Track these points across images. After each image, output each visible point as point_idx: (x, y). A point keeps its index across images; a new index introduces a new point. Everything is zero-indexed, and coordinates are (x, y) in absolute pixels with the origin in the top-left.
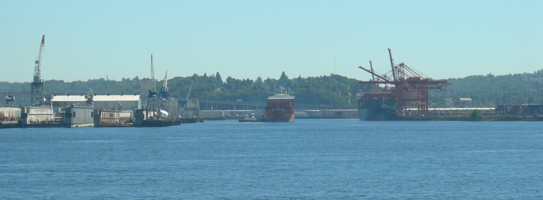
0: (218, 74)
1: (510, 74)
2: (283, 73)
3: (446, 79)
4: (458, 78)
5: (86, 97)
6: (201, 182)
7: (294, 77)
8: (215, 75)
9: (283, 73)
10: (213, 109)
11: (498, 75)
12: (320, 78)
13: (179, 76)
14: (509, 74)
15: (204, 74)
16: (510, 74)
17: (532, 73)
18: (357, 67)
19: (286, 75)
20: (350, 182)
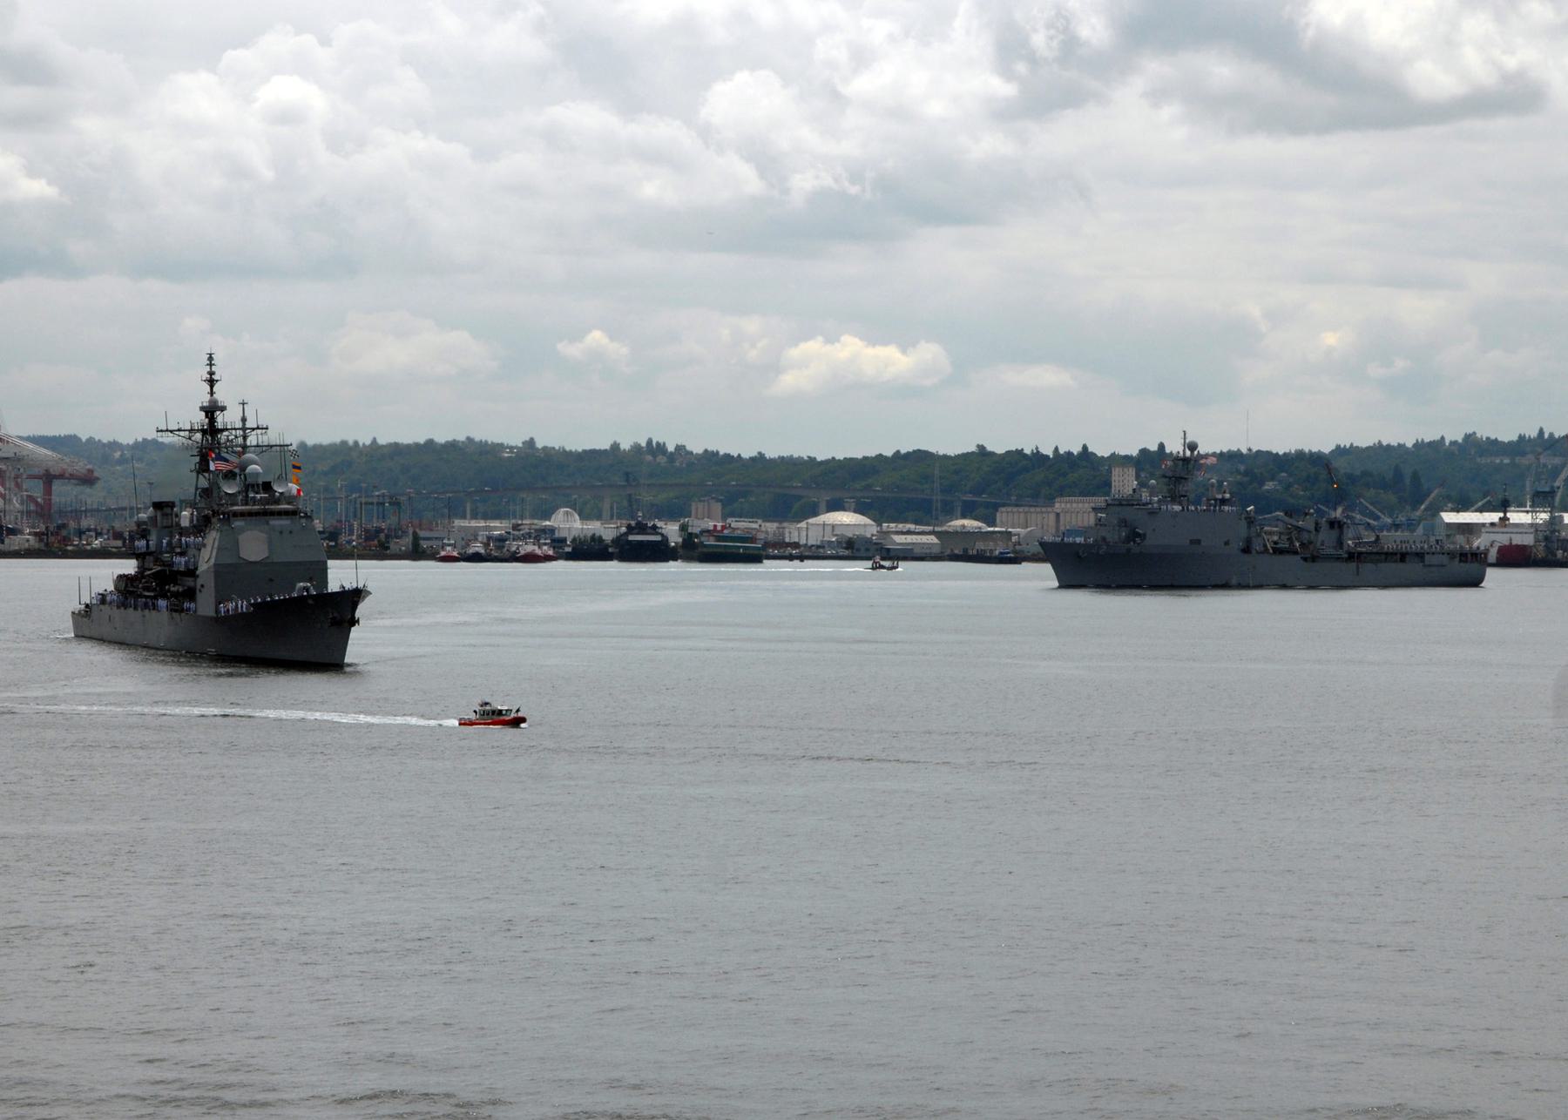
0: (532, 439)
1: (615, 446)
2: (375, 439)
3: (1232, 449)
4: (1463, 436)
5: (299, 491)
6: (24, 970)
7: (834, 456)
8: (644, 444)
9: (375, 439)
10: (165, 570)
11: (1360, 446)
12: (1413, 449)
13: (926, 449)
14: (1377, 442)
15: (1080, 449)
16: (615, 446)
17: (1345, 446)
18: (1057, 444)
19: (1090, 450)
20: (818, 943)
